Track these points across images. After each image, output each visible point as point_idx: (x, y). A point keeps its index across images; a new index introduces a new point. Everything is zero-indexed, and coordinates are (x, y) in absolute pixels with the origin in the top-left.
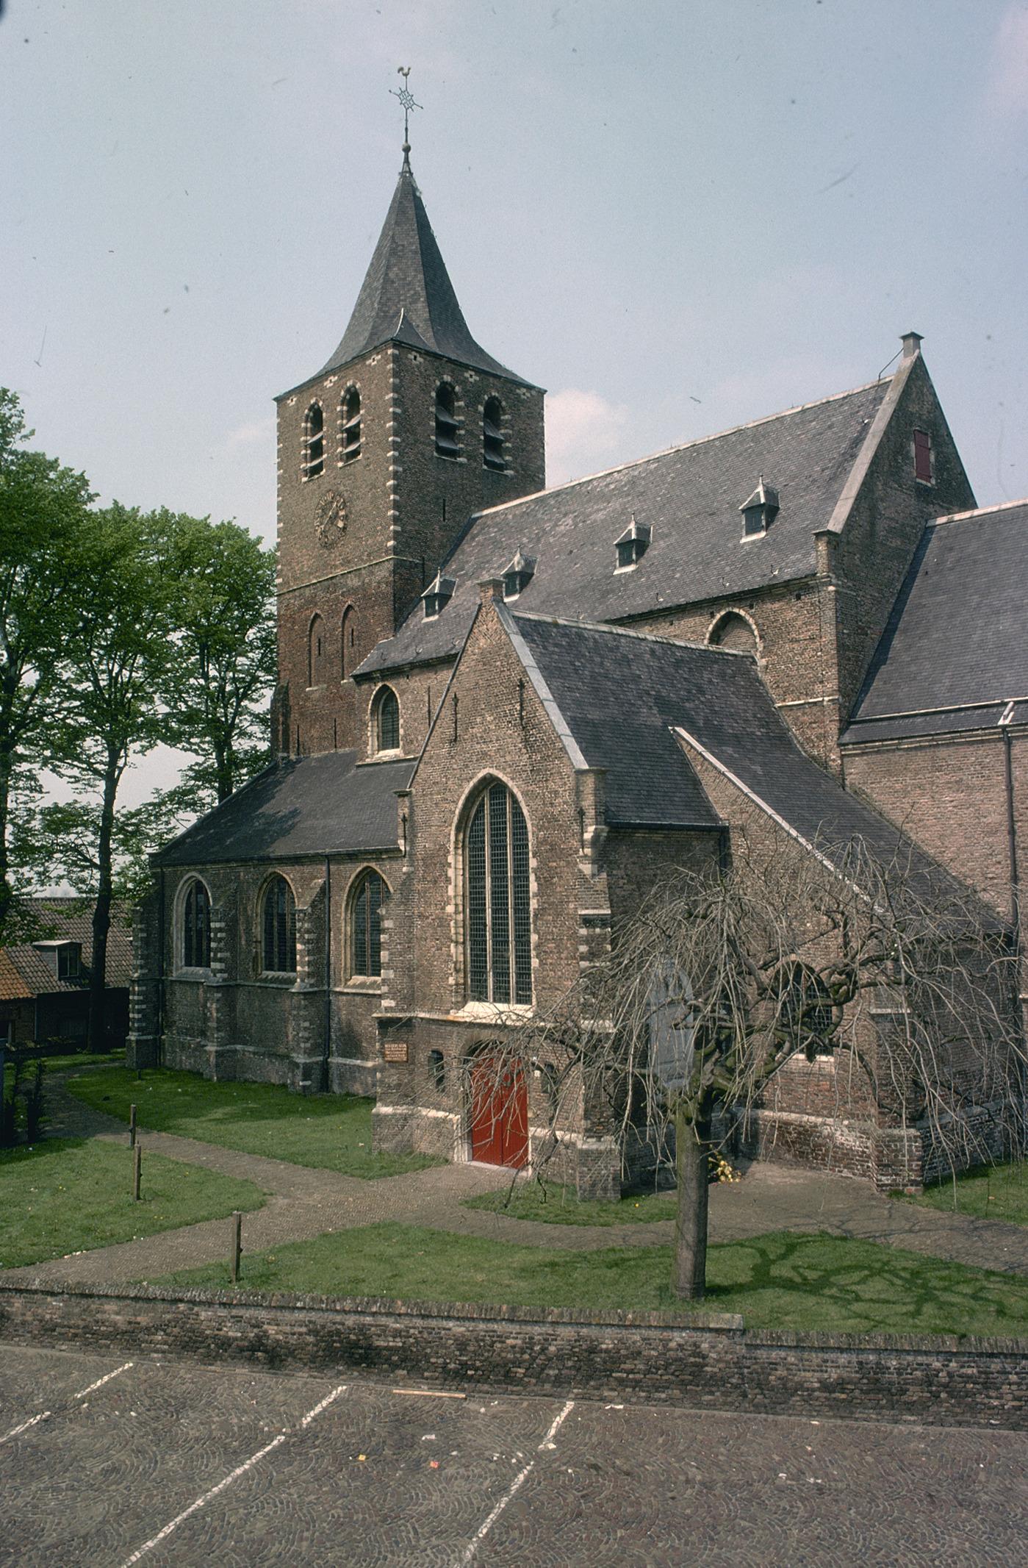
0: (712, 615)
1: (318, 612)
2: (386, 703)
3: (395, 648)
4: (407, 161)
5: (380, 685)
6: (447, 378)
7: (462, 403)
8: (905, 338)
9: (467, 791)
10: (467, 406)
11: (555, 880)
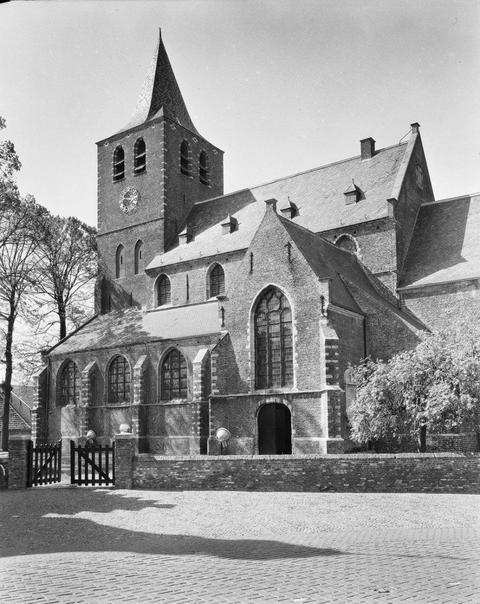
0: (335, 237)
1: (121, 243)
3: (160, 260)
6: (186, 139)
8: (412, 125)
9: (258, 293)
11: (308, 328)
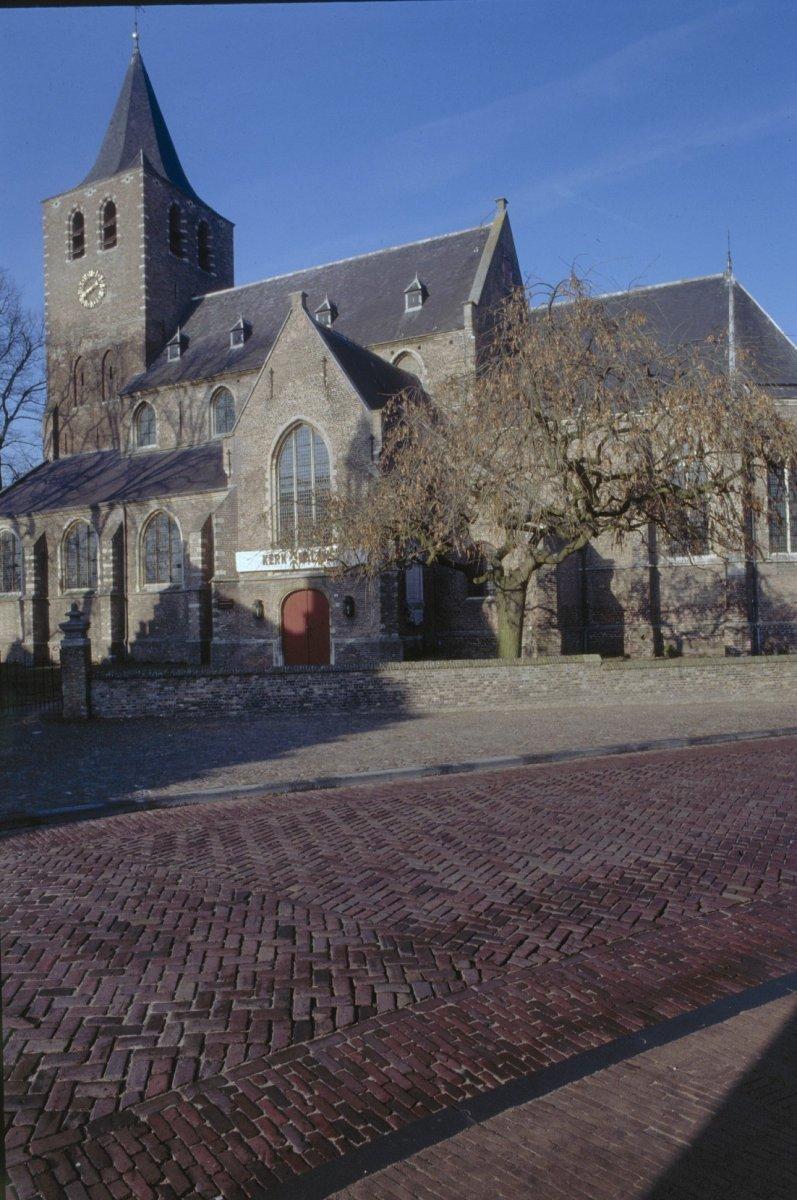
6: (177, 202)
10: (188, 223)
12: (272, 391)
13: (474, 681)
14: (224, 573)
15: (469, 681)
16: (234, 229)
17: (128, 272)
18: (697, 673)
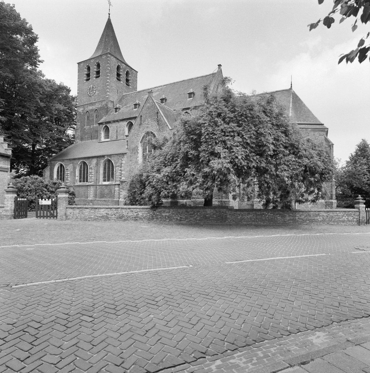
2: (107, 130)
4: (109, 17)
5: (105, 125)
6: (119, 64)
7: (122, 70)
12: (141, 122)
13: (192, 213)
14: (124, 178)
15: (190, 213)
16: (334, 146)
17: (103, 85)
18: (266, 214)
